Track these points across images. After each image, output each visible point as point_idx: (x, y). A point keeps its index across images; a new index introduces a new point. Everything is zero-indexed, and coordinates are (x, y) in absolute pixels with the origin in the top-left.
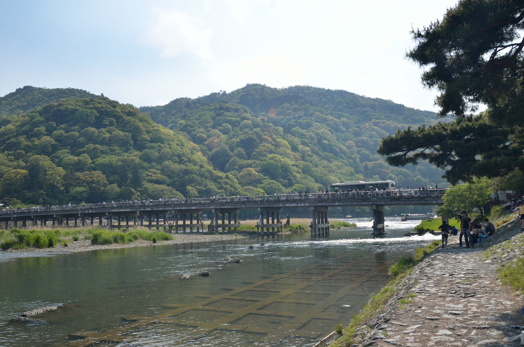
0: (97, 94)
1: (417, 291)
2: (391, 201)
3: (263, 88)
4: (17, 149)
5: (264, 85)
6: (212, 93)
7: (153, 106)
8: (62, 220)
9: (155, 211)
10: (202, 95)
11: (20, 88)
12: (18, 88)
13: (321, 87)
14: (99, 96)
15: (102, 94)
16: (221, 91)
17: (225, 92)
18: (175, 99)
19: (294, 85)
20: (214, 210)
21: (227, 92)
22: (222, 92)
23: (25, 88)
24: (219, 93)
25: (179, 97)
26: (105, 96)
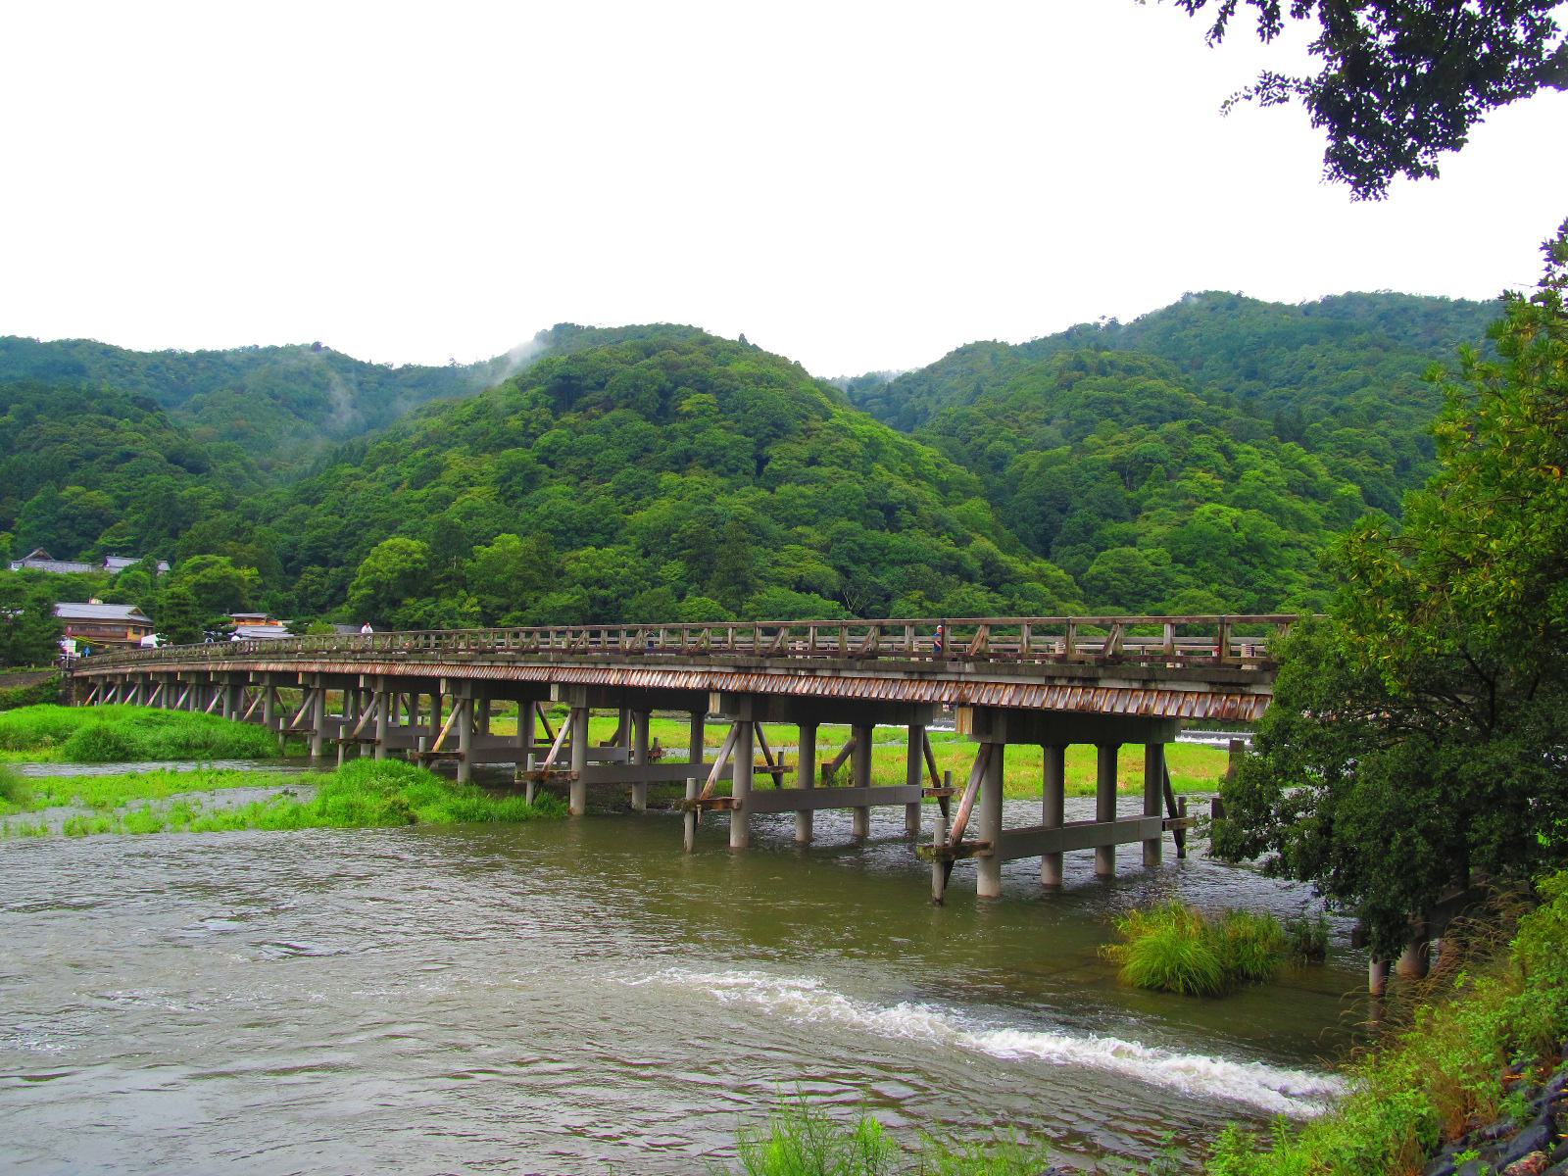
1: (335, 1099)
2: (1052, 687)
3: (1234, 303)
5: (1239, 295)
8: (485, 705)
10: (675, 322)
13: (1436, 292)
14: (733, 341)
15: (742, 337)
16: (1103, 317)
17: (1114, 323)
18: (960, 346)
20: (557, 686)
21: (1123, 322)
22: (1106, 322)
24: (1097, 325)
25: (970, 342)
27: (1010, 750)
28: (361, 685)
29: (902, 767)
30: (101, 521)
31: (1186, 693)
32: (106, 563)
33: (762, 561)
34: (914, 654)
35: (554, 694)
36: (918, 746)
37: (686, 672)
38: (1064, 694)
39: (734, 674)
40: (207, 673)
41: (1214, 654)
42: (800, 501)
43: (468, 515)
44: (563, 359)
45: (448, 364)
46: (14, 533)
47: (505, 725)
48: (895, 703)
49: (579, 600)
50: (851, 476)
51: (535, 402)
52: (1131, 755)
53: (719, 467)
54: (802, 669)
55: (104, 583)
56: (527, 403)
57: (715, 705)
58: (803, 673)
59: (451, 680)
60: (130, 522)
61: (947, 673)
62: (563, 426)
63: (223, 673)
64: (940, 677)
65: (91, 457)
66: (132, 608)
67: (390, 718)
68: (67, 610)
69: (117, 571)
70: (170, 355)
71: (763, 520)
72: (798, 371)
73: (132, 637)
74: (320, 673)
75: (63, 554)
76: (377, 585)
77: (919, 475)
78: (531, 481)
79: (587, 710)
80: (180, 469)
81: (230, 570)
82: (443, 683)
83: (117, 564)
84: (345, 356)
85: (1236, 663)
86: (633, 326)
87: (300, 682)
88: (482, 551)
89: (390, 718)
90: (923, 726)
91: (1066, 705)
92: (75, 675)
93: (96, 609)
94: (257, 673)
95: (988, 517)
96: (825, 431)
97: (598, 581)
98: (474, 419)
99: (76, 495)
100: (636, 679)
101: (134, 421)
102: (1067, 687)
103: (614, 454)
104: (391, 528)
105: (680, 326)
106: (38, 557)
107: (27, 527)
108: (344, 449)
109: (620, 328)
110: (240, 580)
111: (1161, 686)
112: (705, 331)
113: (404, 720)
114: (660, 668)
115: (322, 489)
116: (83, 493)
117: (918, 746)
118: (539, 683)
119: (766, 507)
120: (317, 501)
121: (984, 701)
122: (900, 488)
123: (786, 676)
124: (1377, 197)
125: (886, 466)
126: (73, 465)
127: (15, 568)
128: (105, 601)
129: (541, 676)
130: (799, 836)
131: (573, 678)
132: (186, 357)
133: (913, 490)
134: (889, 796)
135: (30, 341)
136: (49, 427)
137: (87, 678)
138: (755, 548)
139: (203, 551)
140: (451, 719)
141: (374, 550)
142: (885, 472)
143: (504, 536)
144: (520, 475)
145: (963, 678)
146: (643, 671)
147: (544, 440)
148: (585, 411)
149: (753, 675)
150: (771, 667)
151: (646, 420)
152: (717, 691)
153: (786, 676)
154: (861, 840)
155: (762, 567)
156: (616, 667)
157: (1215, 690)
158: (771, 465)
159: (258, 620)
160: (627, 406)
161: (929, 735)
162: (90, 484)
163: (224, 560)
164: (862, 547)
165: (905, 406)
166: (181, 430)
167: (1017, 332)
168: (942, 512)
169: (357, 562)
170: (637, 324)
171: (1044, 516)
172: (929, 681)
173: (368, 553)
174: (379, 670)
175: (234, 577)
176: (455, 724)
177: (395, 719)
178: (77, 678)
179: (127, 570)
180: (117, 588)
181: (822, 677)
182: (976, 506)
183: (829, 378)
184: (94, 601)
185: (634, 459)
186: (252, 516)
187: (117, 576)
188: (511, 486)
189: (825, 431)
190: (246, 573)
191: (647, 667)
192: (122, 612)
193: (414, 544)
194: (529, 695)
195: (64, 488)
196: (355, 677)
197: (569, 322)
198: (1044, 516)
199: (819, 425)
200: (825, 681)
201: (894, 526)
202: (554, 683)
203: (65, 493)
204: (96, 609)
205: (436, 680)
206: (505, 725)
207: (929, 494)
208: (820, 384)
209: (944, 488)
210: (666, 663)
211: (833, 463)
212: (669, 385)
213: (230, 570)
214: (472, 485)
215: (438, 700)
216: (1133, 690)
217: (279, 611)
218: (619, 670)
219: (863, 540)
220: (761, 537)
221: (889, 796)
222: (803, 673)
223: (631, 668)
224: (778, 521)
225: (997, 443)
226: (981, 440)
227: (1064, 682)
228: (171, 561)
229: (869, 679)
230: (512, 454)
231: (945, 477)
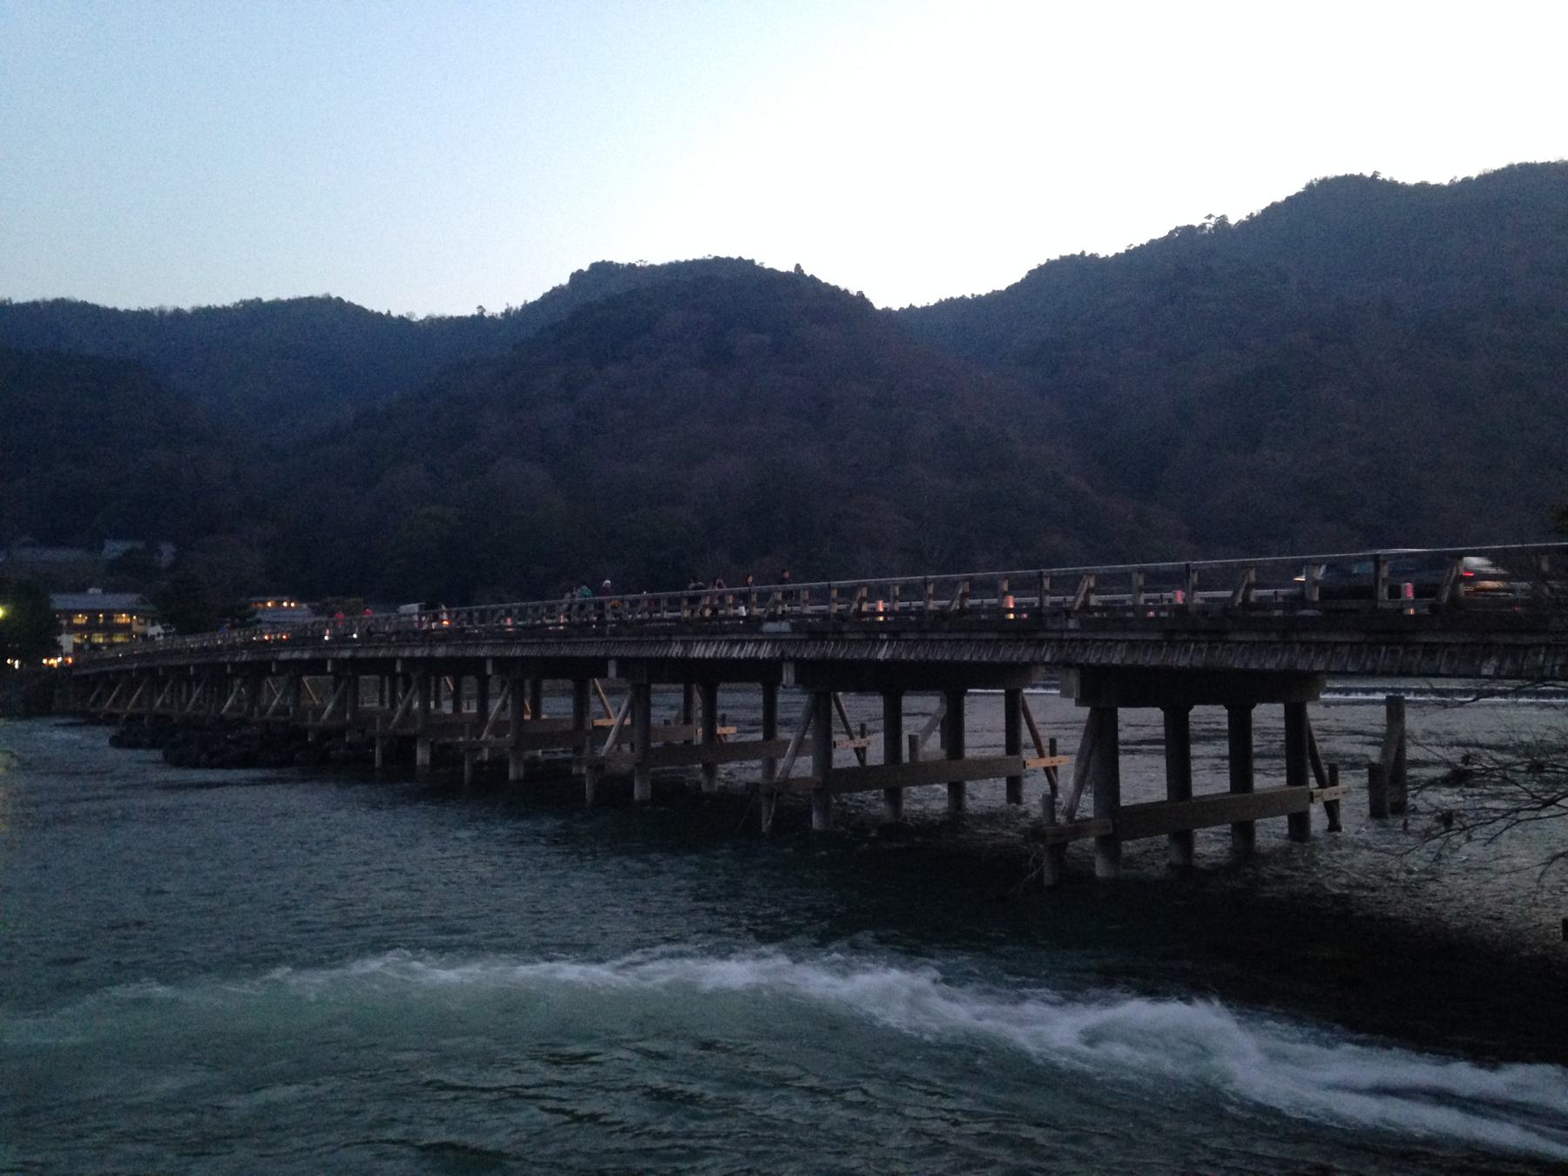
0: (469, 314)
5: (1375, 175)
6: (1177, 229)
7: (977, 294)
9: (1181, 672)
11: (580, 271)
14: (788, 273)
15: (798, 267)
16: (1210, 217)
18: (1043, 262)
19: (691, 259)
21: (1233, 221)
22: (1213, 220)
23: (595, 267)
24: (1203, 227)
25: (1055, 256)
26: (808, 273)
27: (1125, 714)
28: (399, 669)
29: (1000, 737)
31: (1336, 644)
34: (881, 614)
35: (612, 671)
36: (1015, 711)
38: (1187, 651)
39: (807, 641)
41: (1036, 605)
47: (557, 707)
48: (990, 666)
52: (1268, 716)
54: (884, 632)
57: (788, 675)
59: (498, 661)
61: (1046, 630)
64: (1040, 635)
67: (432, 704)
72: (861, 302)
82: (489, 665)
83: (115, 549)
85: (1397, 606)
87: (329, 669)
89: (432, 704)
90: (1019, 691)
91: (1278, 665)
94: (279, 663)
100: (699, 651)
102: (1188, 641)
109: (686, 262)
111: (1304, 637)
112: (757, 263)
113: (447, 708)
114: (726, 637)
117: (1015, 711)
118: (595, 658)
121: (1093, 660)
129: (390, 653)
131: (631, 652)
134: (985, 769)
135: (1152, 242)
137: (87, 676)
140: (499, 702)
145: (1066, 636)
146: (709, 641)
149: (829, 641)
150: (849, 631)
152: (790, 659)
153: (866, 640)
156: (678, 638)
157: (1371, 639)
161: (1027, 698)
167: (1108, 243)
172: (1028, 640)
174: (418, 653)
176: (504, 707)
177: (438, 705)
181: (907, 640)
184: (91, 591)
191: (713, 637)
194: (581, 674)
196: (393, 660)
202: (611, 658)
205: (481, 661)
206: (557, 707)
215: (484, 681)
216: (1271, 643)
218: (681, 641)
221: (985, 769)
222: (885, 636)
227: (1185, 636)
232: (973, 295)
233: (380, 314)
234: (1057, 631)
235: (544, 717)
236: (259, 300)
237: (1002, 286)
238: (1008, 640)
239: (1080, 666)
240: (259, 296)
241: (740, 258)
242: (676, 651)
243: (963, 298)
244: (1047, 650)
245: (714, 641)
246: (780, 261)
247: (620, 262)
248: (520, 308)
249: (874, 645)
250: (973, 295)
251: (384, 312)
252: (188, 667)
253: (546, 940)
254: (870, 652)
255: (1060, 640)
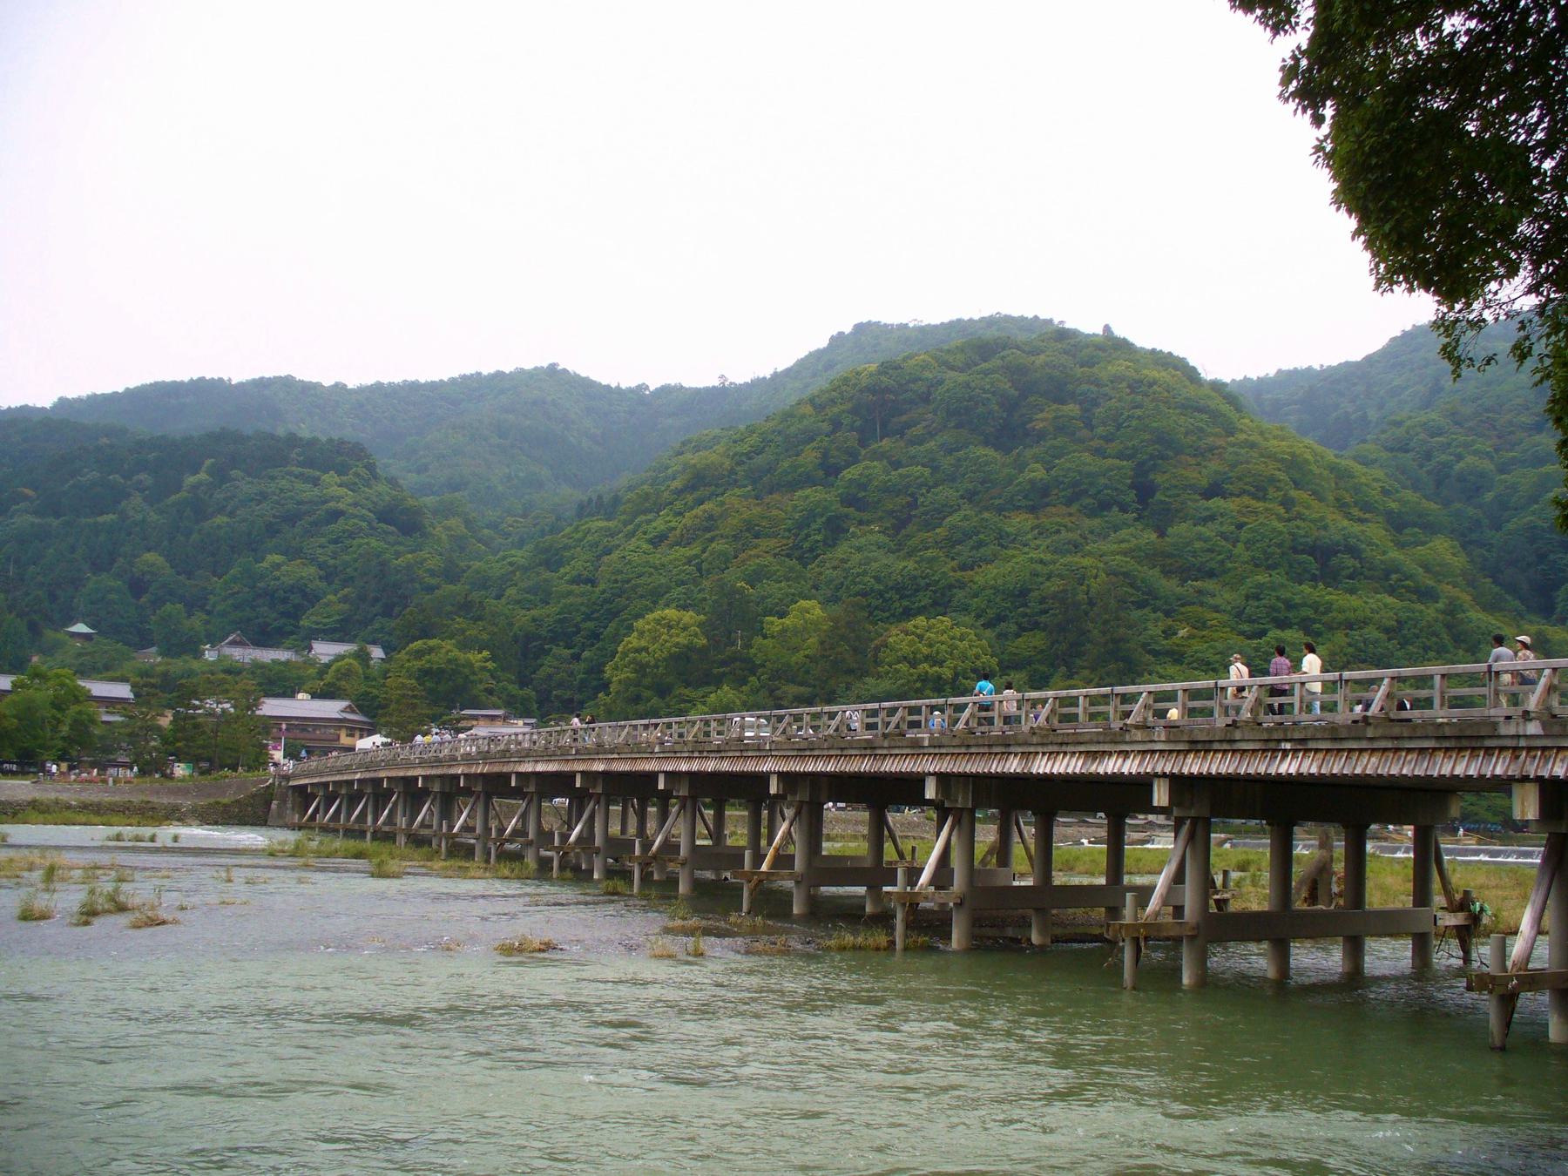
4: (712, 540)
11: (841, 334)
12: (835, 333)
15: (1107, 328)
18: (1408, 328)
23: (860, 328)
30: (305, 595)
32: (310, 649)
33: (1154, 630)
37: (1120, 752)
39: (1189, 751)
40: (456, 777)
42: (1198, 545)
43: (754, 579)
44: (873, 367)
45: (716, 383)
46: (208, 613)
49: (903, 685)
50: (1267, 509)
51: (836, 424)
53: (1087, 501)
54: (1287, 740)
55: (312, 671)
56: (826, 427)
58: (1288, 746)
60: (333, 603)
62: (877, 456)
63: (476, 776)
65: (291, 519)
66: (345, 704)
68: (272, 707)
69: (325, 660)
70: (378, 387)
71: (1153, 575)
73: (345, 740)
74: (605, 773)
75: (264, 638)
76: (641, 668)
77: (1367, 507)
78: (836, 529)
79: (972, 811)
80: (392, 528)
81: (456, 653)
83: (325, 651)
84: (587, 379)
86: (959, 321)
88: (774, 624)
92: (291, 783)
93: (303, 706)
95: (1458, 561)
96: (1231, 449)
97: (927, 658)
98: (759, 452)
99: (278, 566)
100: (1041, 766)
101: (340, 474)
103: (946, 493)
104: (656, 597)
105: (1022, 319)
106: (234, 643)
107: (219, 608)
108: (590, 500)
110: (470, 665)
112: (1056, 322)
114: (1082, 748)
115: (567, 548)
116: (284, 563)
117: (1426, 858)
119: (1151, 557)
120: (560, 564)
122: (1339, 526)
123: (1264, 751)
124: (1286, 32)
125: (1314, 493)
126: (272, 530)
127: (210, 655)
128: (314, 696)
130: (1271, 973)
132: (936, 326)
133: (1356, 528)
134: (1389, 924)
135: (464, 377)
136: (246, 487)
138: (1139, 613)
139: (425, 634)
141: (639, 624)
142: (1315, 504)
143: (803, 603)
144: (819, 521)
145: (1523, 743)
146: (1058, 753)
147: (850, 473)
148: (902, 434)
151: (986, 443)
152: (1164, 775)
153: (1264, 751)
154: (1355, 977)
155: (1152, 637)
158: (1159, 496)
159: (493, 718)
160: (958, 426)
162: (293, 553)
163: (448, 645)
164: (1290, 606)
165: (1334, 415)
166: (393, 482)
168: (1394, 554)
169: (616, 638)
170: (966, 318)
171: (1542, 557)
173: (630, 628)
175: (463, 662)
178: (294, 787)
179: (339, 658)
180: (328, 678)
182: (1442, 548)
183: (1228, 380)
184: (300, 696)
185: (970, 496)
186: (483, 583)
187: (328, 666)
188: (808, 536)
189: (1231, 449)
190: (476, 658)
191: (1064, 748)
192: (331, 709)
193: (688, 617)
195: (263, 559)
197: (874, 320)
198: (1542, 557)
199: (1220, 442)
200: (1320, 756)
201: (1330, 577)
203: (264, 565)
204: (303, 706)
207: (1375, 531)
208: (1217, 386)
209: (1397, 524)
210: (1091, 742)
211: (1242, 493)
212: (1014, 393)
213: (456, 653)
214: (757, 537)
217: (518, 709)
219: (1288, 595)
220: (1148, 599)
222: (1288, 746)
223: (1040, 749)
224: (1167, 573)
225: (1470, 459)
226: (1444, 458)
228: (388, 648)
229: (1385, 750)
230: (813, 495)
231: (1393, 505)
232: (1322, 366)
233: (608, 387)
234: (1513, 737)
235: (824, 853)
236: (479, 374)
237: (1357, 356)
238: (1447, 749)
239: (1539, 780)
240: (60, 395)
241: (1036, 317)
242: (1013, 766)
243: (1309, 369)
244: (1498, 758)
245: (1065, 753)
246: (1088, 323)
247: (889, 322)
248: (768, 377)
249: (1273, 758)
250: (1322, 366)
251: (613, 385)
252: (416, 778)
253: (752, 1156)
254: (1269, 765)
255: (1515, 749)
